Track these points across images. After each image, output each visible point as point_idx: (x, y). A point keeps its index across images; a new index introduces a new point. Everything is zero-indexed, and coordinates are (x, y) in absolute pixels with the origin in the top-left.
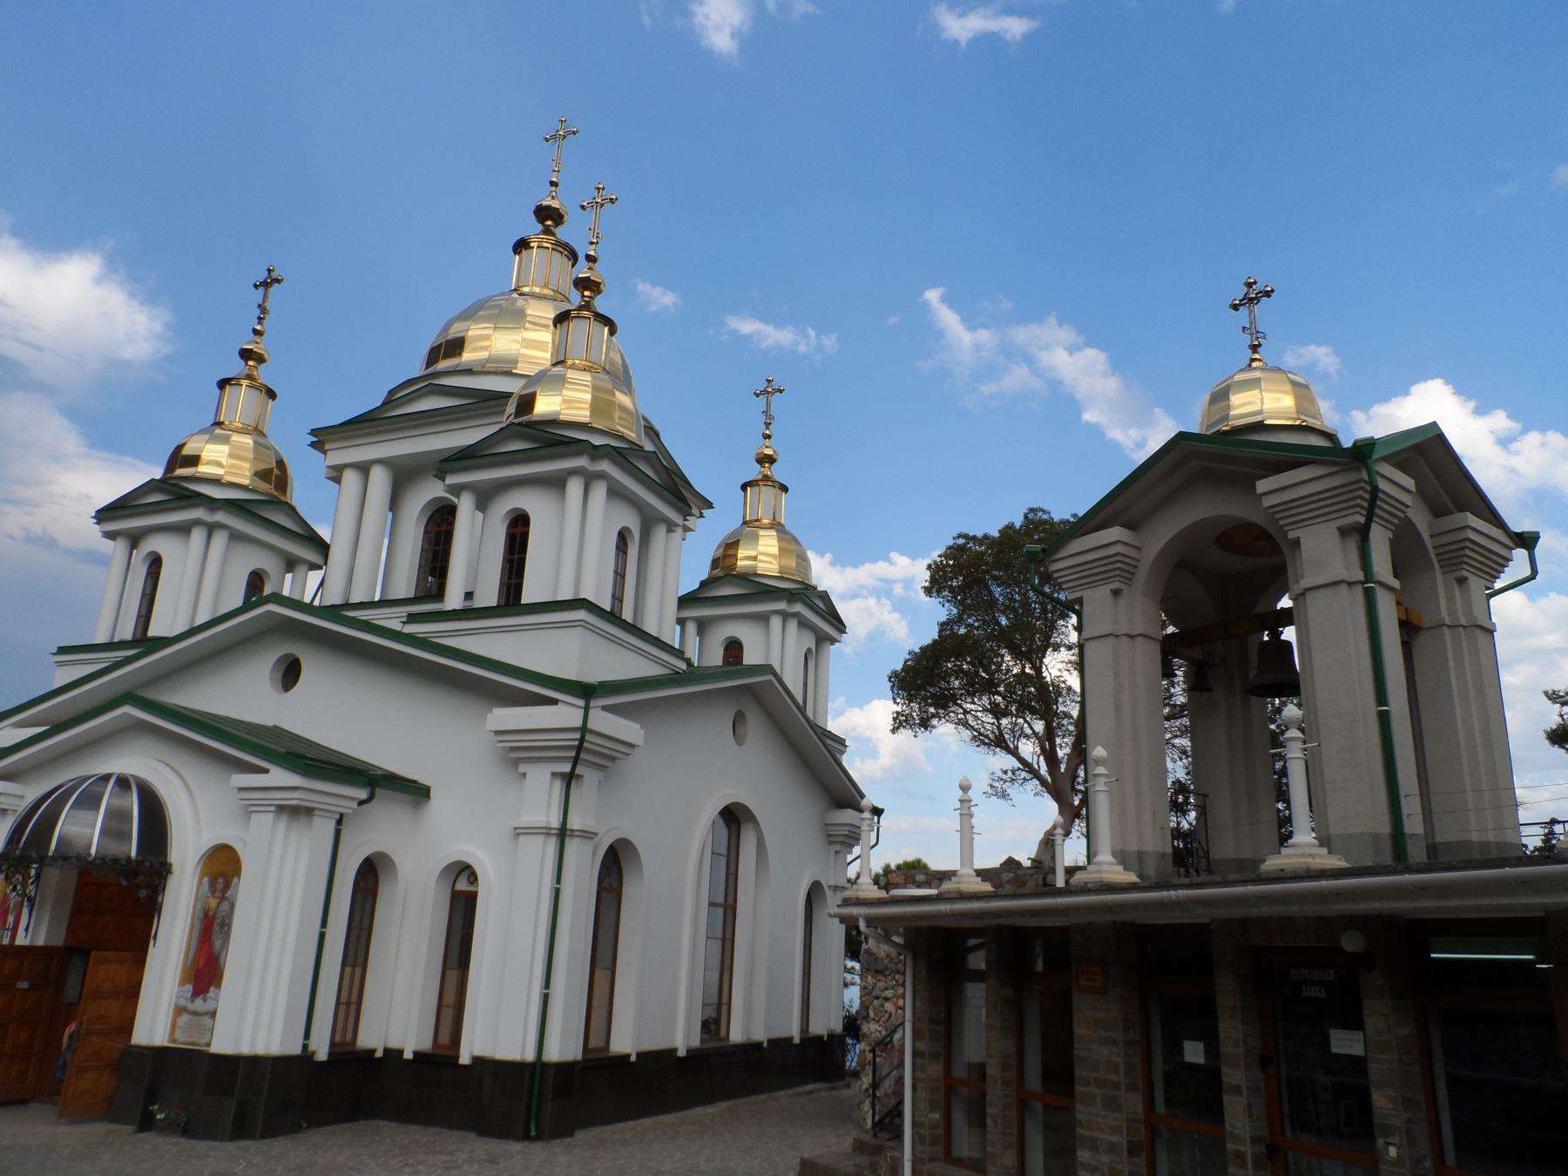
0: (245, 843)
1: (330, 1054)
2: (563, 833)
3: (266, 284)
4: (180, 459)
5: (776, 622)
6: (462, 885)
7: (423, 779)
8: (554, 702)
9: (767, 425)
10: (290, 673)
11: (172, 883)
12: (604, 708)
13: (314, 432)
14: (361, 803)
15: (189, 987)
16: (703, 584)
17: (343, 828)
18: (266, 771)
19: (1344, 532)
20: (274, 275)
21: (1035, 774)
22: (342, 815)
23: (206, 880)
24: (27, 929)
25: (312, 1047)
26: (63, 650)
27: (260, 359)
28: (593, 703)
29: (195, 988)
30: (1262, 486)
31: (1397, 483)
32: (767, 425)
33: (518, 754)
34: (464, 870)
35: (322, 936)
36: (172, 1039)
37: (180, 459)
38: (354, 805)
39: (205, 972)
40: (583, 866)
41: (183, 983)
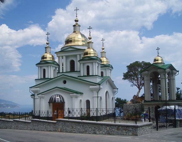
2: (98, 97)
4: (43, 58)
5: (107, 70)
9: (90, 33)
10: (65, 82)
19: (164, 74)
21: (136, 85)
26: (36, 80)
27: (49, 44)
30: (158, 70)
31: (168, 70)
32: (90, 33)
33: (92, 90)
37: (43, 58)
40: (99, 98)
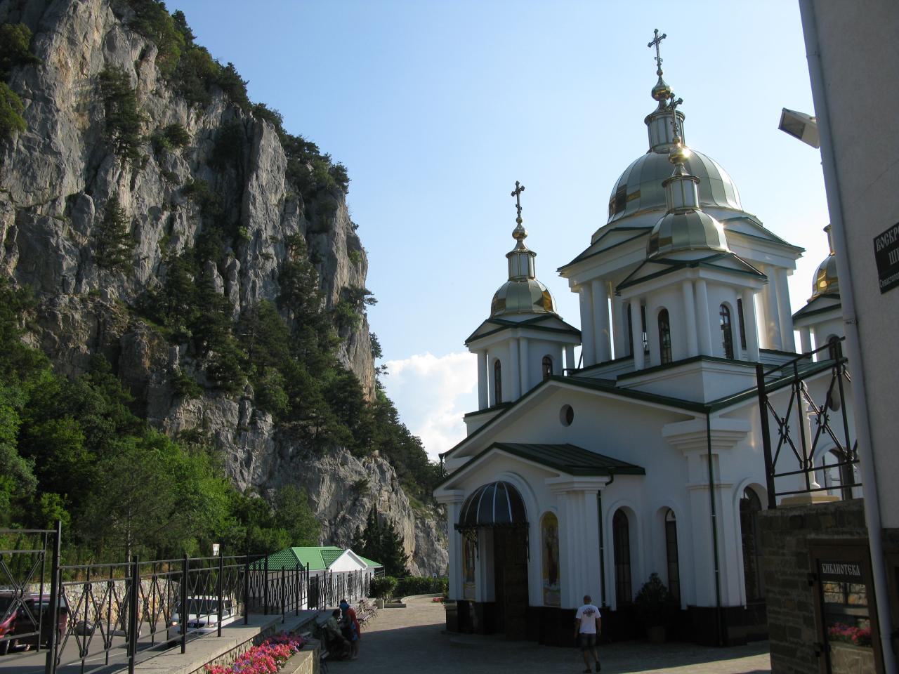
0: (556, 508)
1: (617, 607)
3: (657, 41)
6: (670, 518)
7: (641, 464)
8: (693, 418)
11: (531, 530)
12: (721, 416)
13: (559, 270)
14: (607, 484)
15: (547, 579)
16: (810, 302)
17: (602, 497)
18: (559, 476)
20: (660, 34)
22: (599, 491)
23: (545, 529)
24: (478, 557)
25: (608, 604)
28: (711, 416)
29: (478, 603)
34: (668, 510)
35: (602, 552)
36: (545, 603)
38: (604, 486)
39: (553, 572)
41: (544, 578)
